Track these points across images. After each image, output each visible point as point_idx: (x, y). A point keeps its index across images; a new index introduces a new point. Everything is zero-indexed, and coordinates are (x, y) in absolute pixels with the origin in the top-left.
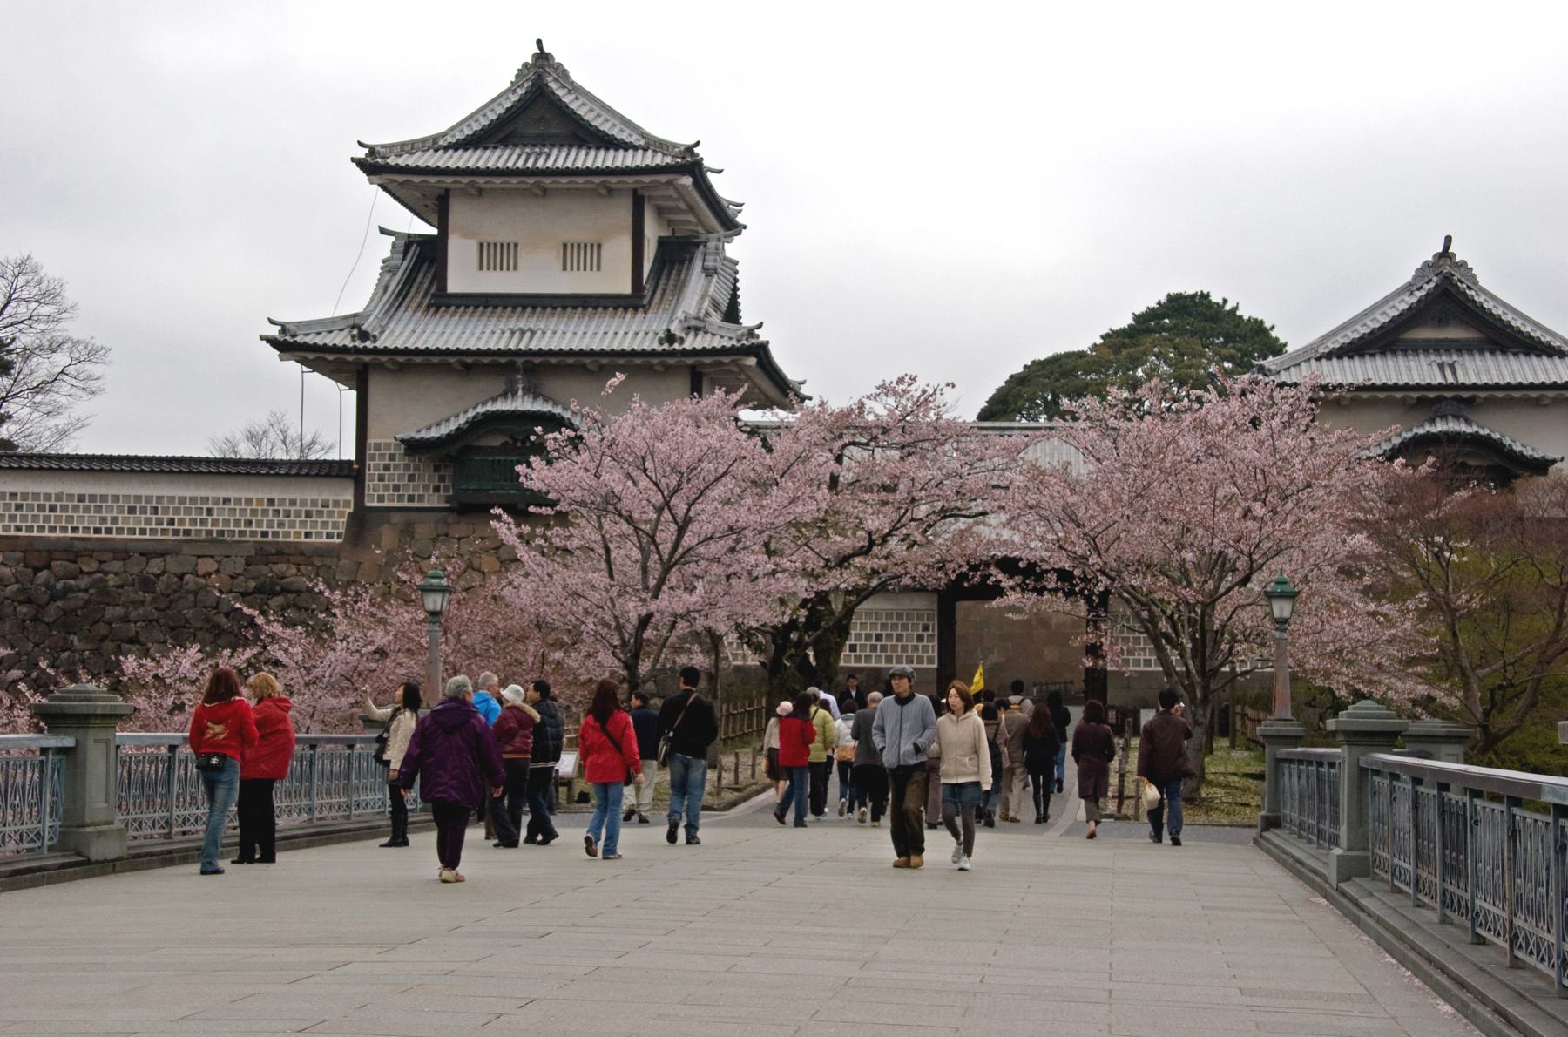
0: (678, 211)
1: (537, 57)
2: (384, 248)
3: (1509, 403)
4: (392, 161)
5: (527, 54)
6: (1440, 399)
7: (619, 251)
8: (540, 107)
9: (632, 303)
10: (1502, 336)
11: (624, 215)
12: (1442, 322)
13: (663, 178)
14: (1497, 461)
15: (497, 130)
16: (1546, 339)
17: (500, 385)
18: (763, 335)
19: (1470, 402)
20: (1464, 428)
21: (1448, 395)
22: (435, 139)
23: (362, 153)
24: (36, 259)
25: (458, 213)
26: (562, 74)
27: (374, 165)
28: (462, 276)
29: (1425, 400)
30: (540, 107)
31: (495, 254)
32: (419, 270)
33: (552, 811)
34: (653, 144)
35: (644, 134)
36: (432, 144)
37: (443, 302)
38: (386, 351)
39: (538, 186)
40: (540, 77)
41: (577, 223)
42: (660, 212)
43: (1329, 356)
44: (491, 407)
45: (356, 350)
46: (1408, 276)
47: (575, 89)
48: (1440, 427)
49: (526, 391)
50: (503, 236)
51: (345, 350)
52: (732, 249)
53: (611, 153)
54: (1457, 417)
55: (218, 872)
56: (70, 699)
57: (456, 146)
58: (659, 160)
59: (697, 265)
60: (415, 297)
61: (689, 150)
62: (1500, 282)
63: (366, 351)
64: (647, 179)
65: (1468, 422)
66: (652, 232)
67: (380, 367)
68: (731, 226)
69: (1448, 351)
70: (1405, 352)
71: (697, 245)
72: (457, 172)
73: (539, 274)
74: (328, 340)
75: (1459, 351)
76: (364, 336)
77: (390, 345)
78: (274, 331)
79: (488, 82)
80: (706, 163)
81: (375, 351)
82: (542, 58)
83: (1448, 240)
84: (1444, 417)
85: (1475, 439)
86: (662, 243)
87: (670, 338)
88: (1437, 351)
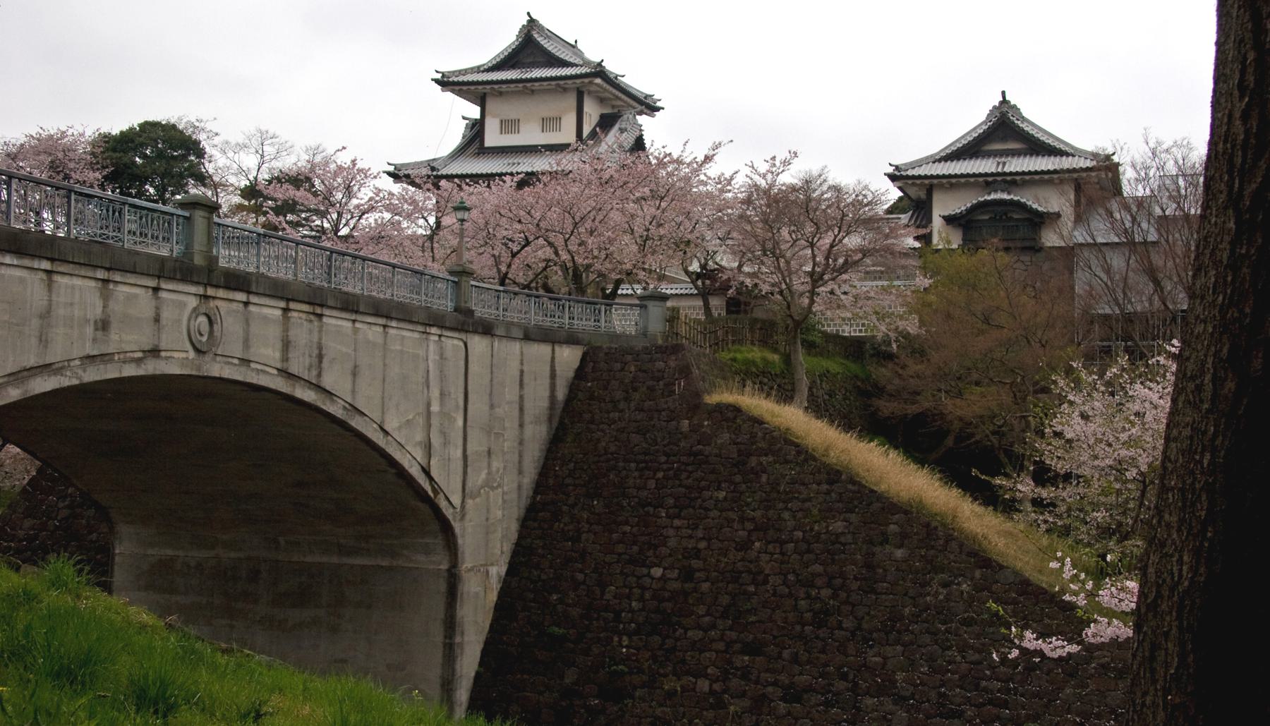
0: (611, 102)
1: (1001, 103)
3: (1042, 183)
5: (524, 20)
6: (995, 181)
7: (570, 121)
8: (531, 47)
10: (1037, 146)
11: (572, 101)
12: (1004, 139)
13: (586, 80)
14: (1027, 216)
15: (510, 60)
16: (1062, 146)
19: (1014, 183)
20: (1005, 196)
21: (999, 179)
22: (479, 67)
24: (324, 145)
25: (490, 105)
26: (541, 29)
27: (446, 82)
28: (493, 138)
29: (989, 182)
30: (531, 47)
31: (509, 126)
32: (474, 140)
35: (1072, 147)
36: (478, 70)
39: (527, 89)
41: (549, 106)
43: (940, 161)
46: (983, 118)
47: (1024, 119)
48: (993, 196)
50: (513, 116)
53: (1058, 159)
54: (1003, 191)
58: (1089, 164)
60: (473, 149)
61: (600, 64)
62: (1041, 114)
65: (1009, 193)
69: (1001, 156)
70: (983, 157)
72: (488, 83)
73: (530, 135)
75: (1007, 156)
76: (433, 169)
79: (505, 38)
82: (532, 22)
83: (1003, 93)
84: (996, 191)
85: (1012, 202)
88: (995, 156)
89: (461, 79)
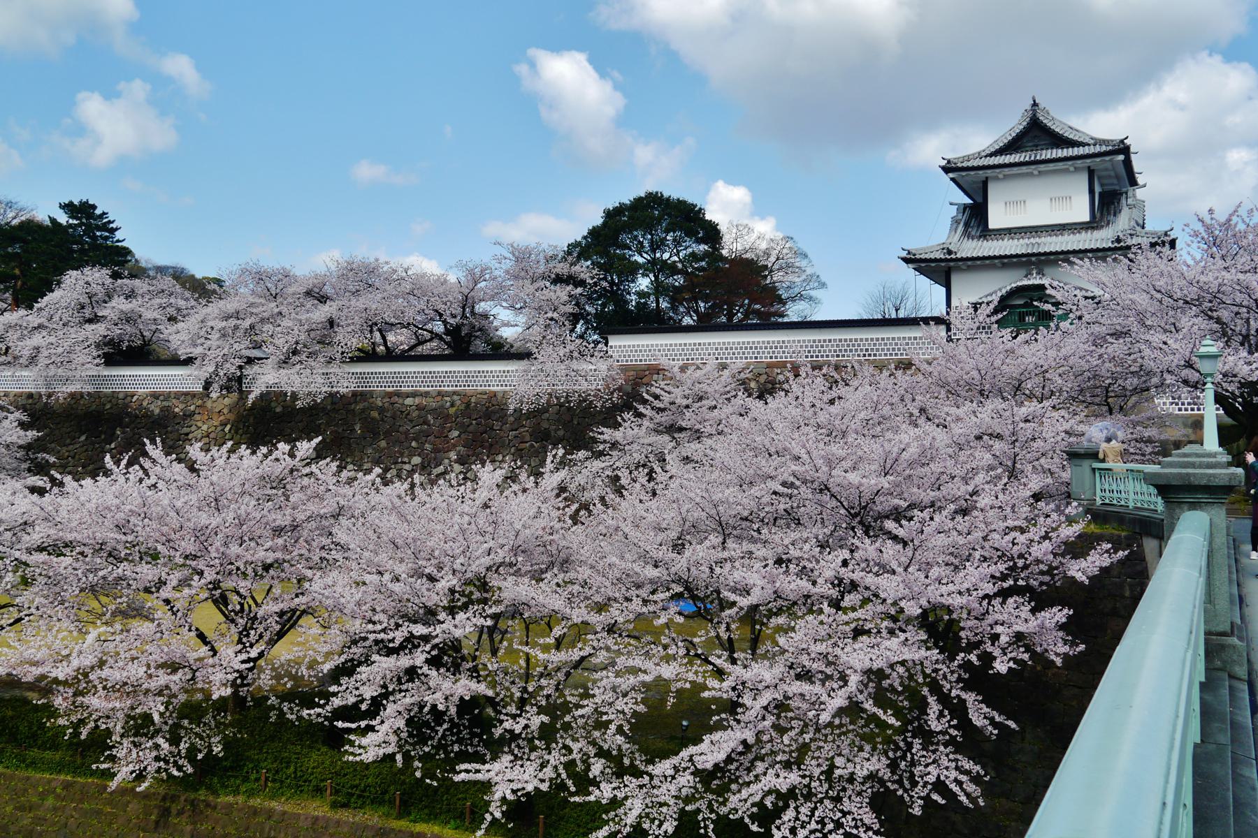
2: (953, 211)
4: (960, 165)
8: (1036, 134)
9: (1093, 224)
13: (1107, 158)
17: (1023, 272)
18: (1173, 235)
23: (944, 163)
28: (996, 219)
30: (1036, 134)
32: (975, 217)
33: (1229, 512)
34: (1099, 142)
37: (986, 233)
38: (962, 259)
40: (1034, 111)
42: (1099, 178)
44: (1020, 284)
45: (946, 260)
49: (1038, 273)
51: (941, 260)
52: (1140, 193)
55: (69, 208)
56: (1193, 465)
57: (991, 155)
58: (1104, 148)
59: (1123, 201)
61: (1122, 141)
63: (952, 260)
64: (1098, 160)
66: (1097, 189)
67: (959, 269)
68: (1133, 183)
71: (1121, 194)
74: (932, 256)
76: (950, 252)
77: (964, 255)
78: (904, 254)
79: (1011, 124)
80: (1132, 150)
81: (957, 260)
82: (1035, 104)
86: (1100, 194)
87: (1118, 240)
89: (970, 164)
